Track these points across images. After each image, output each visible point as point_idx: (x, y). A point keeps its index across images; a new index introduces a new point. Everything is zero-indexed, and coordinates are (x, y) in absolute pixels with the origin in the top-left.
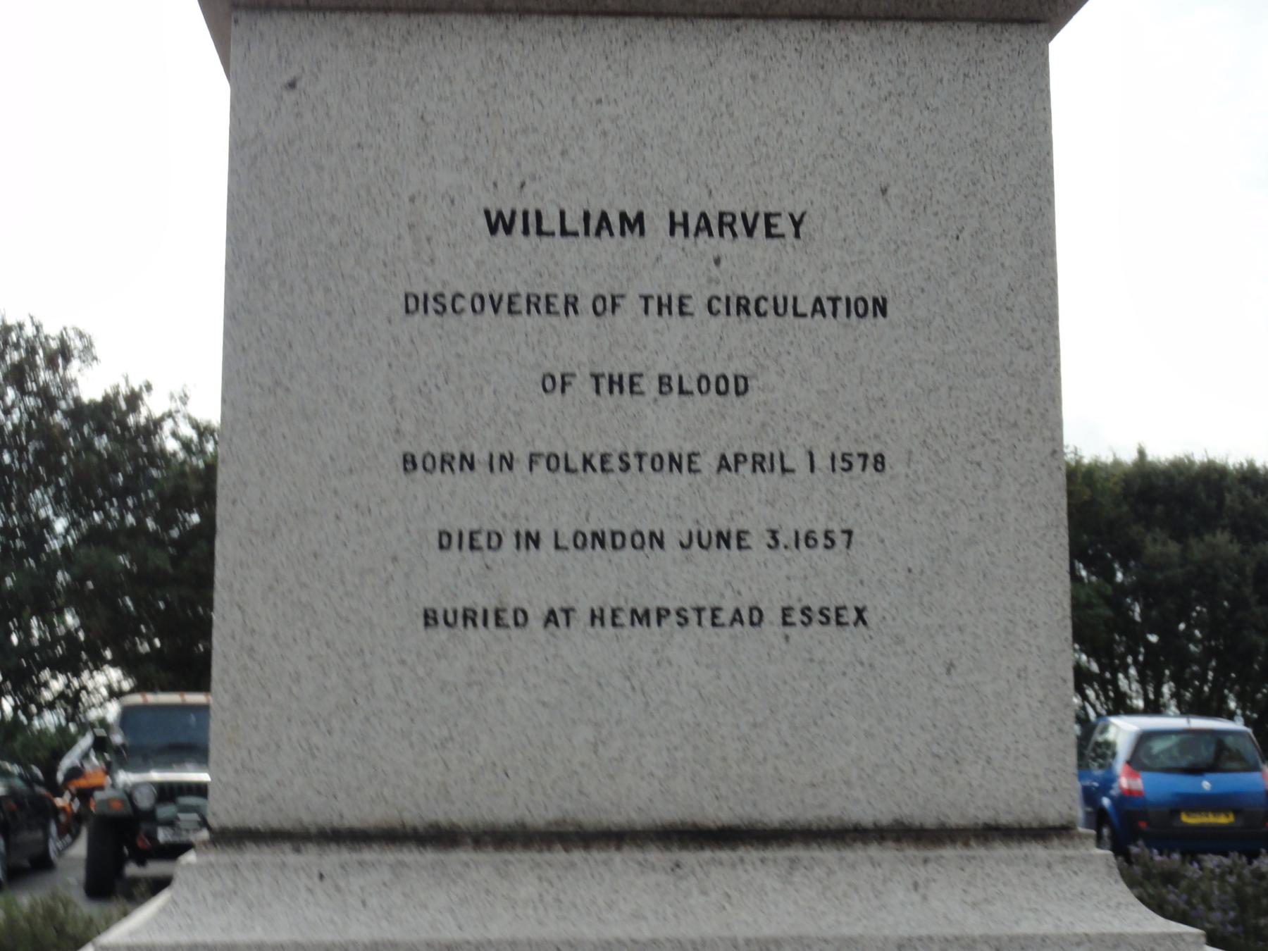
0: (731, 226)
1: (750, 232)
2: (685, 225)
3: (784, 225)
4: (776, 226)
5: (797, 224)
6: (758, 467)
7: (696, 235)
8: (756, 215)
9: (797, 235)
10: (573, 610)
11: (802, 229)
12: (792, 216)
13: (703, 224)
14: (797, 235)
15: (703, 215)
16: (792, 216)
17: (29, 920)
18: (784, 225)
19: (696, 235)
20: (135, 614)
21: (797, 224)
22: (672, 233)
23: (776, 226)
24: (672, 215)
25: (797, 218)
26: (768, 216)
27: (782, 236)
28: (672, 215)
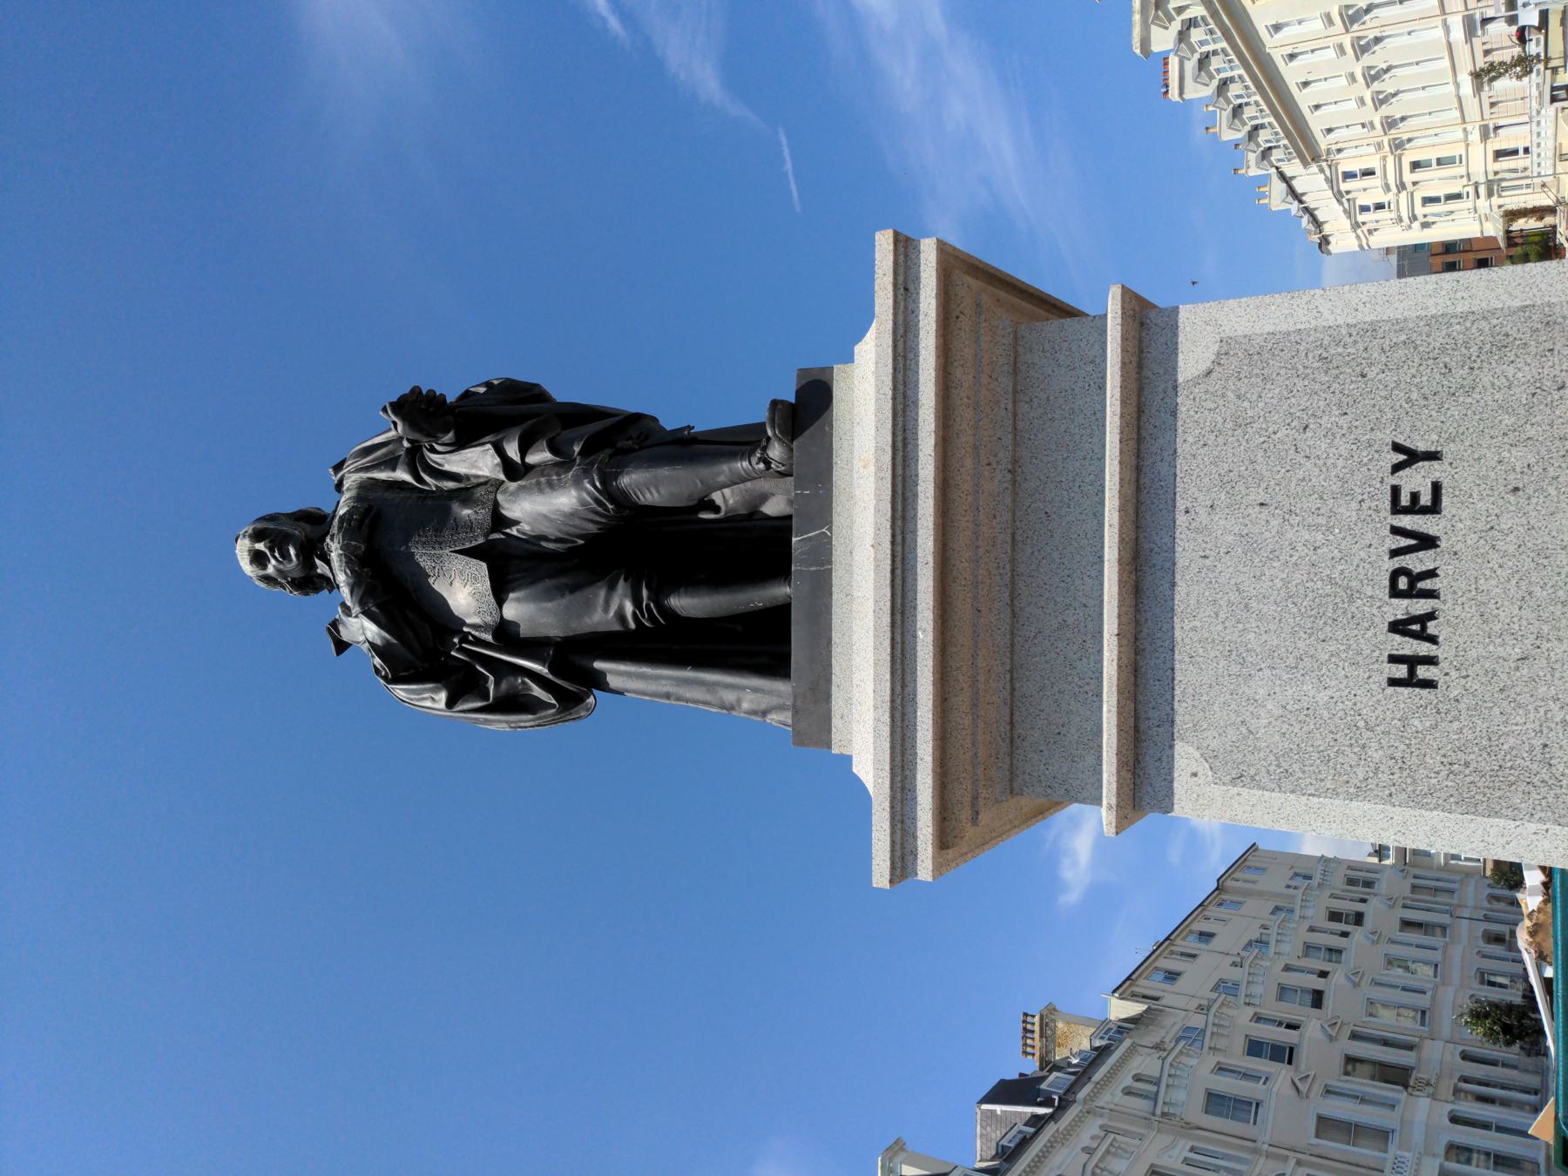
0: (1414, 578)
1: (1427, 542)
2: (1413, 662)
3: (1416, 480)
4: (1415, 497)
5: (1412, 457)
6: (1422, 585)
7: (1433, 640)
8: (1396, 531)
9: (1433, 456)
10: (293, 538)
11: (1421, 446)
12: (1397, 468)
13: (1416, 627)
14: (1433, 456)
15: (1397, 627)
16: (1397, 468)
17: (586, 472)
18: (1416, 480)
19: (1433, 640)
20: (1072, 897)
21: (1412, 457)
22: (1429, 684)
23: (1415, 497)
24: (1393, 682)
25: (1402, 457)
26: (1396, 509)
27: (1436, 488)
28: (1393, 682)
